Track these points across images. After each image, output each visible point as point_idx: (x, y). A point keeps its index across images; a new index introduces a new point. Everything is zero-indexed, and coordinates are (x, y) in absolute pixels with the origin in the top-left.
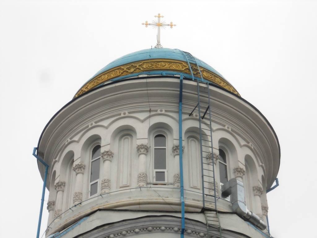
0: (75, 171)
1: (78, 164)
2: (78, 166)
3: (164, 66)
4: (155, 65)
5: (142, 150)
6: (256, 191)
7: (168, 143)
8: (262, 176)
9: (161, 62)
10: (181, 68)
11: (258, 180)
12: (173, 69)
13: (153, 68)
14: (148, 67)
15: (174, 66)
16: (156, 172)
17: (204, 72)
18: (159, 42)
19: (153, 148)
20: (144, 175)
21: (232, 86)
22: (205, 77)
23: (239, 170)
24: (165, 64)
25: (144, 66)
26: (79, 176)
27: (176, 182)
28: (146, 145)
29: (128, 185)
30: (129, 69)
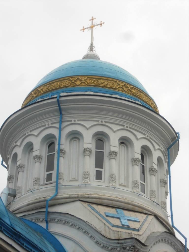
0: (34, 159)
1: (38, 155)
2: (37, 156)
3: (102, 84)
4: (96, 82)
5: (87, 152)
6: (162, 183)
7: (105, 147)
8: (167, 169)
9: (101, 79)
10: (115, 86)
11: (165, 174)
12: (106, 80)
13: (95, 84)
14: (91, 83)
15: (110, 84)
16: (96, 171)
17: (133, 89)
18: (92, 48)
19: (94, 150)
20: (88, 173)
21: (152, 99)
22: (133, 93)
23: (154, 170)
24: (103, 82)
25: (88, 81)
26: (37, 164)
27: (111, 181)
28: (90, 149)
29: (76, 179)
30: (75, 81)
